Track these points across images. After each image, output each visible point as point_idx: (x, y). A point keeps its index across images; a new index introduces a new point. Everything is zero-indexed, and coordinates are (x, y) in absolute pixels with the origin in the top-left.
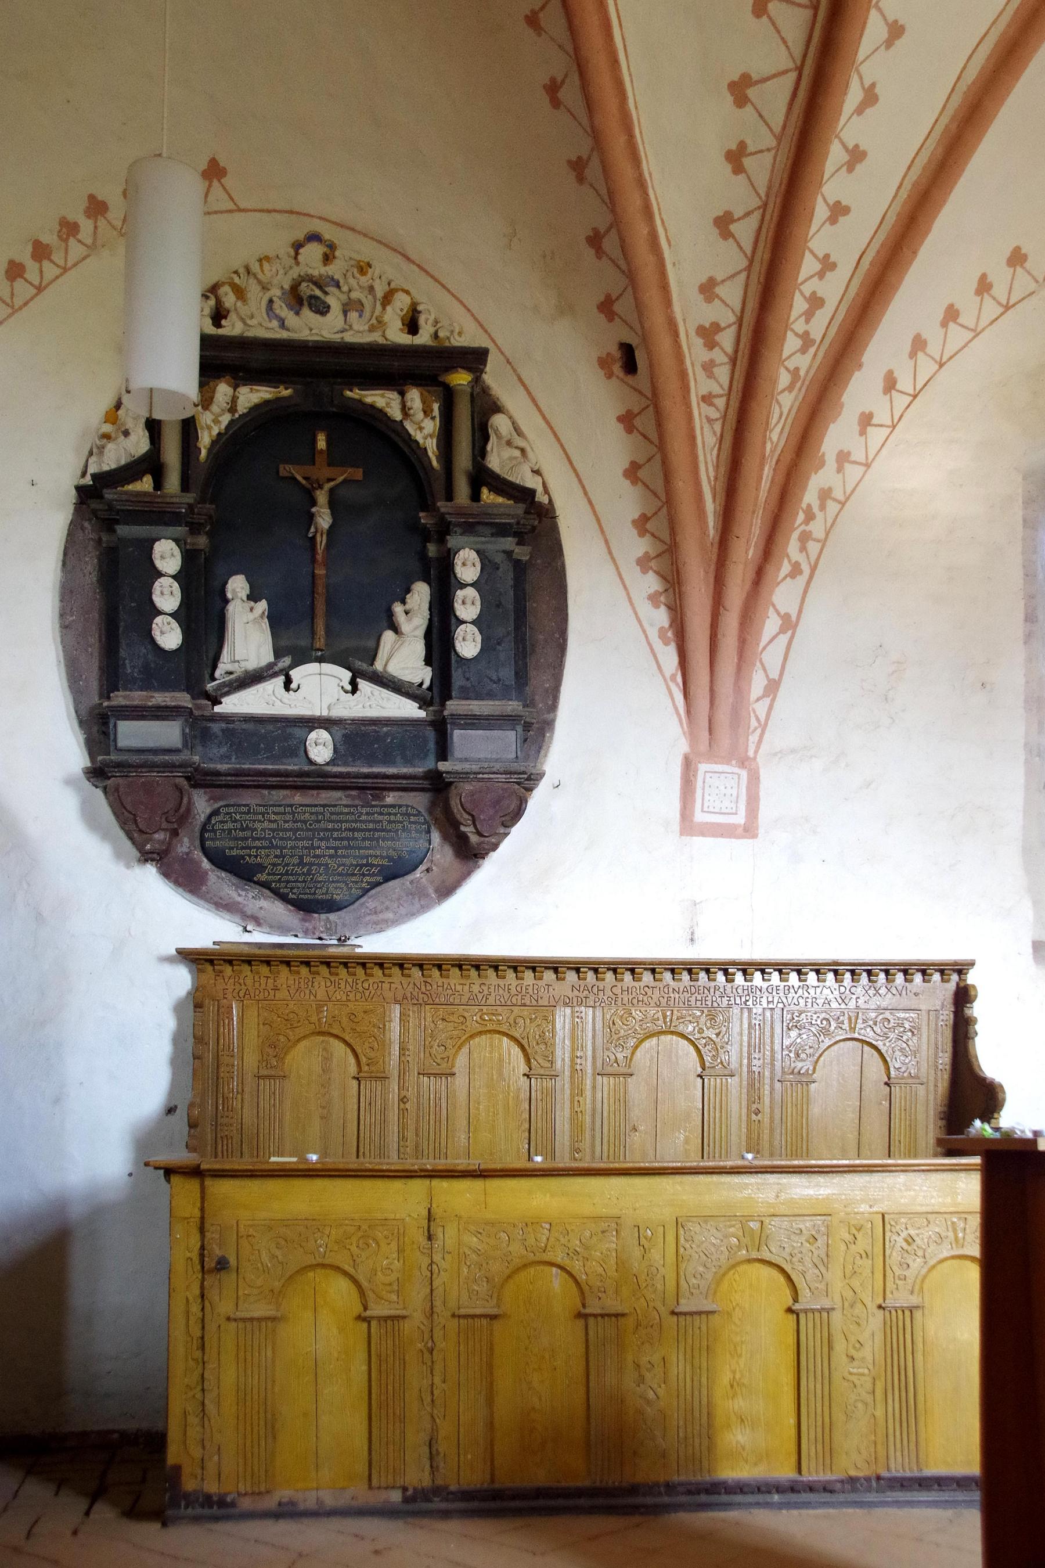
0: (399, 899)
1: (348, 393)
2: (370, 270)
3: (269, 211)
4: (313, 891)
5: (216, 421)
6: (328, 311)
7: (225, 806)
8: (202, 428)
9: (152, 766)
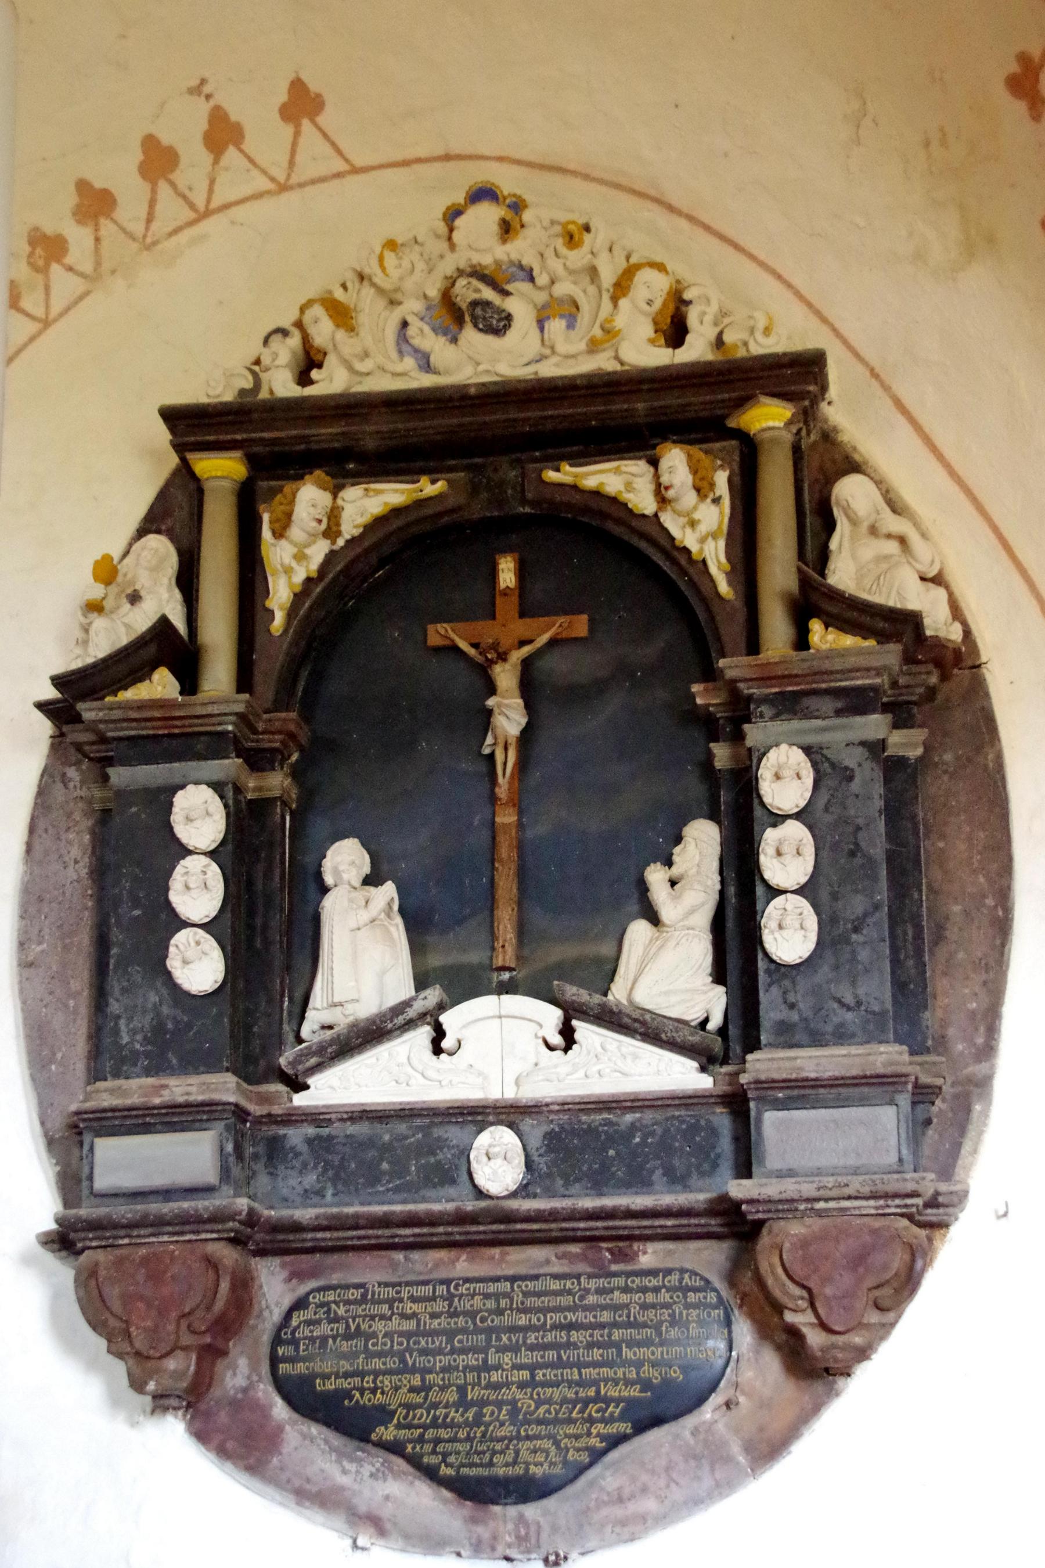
0: (668, 1469)
1: (551, 475)
2: (587, 238)
3: (406, 163)
4: (487, 1458)
5: (300, 557)
6: (507, 327)
7: (319, 1290)
8: (275, 573)
9: (159, 1223)
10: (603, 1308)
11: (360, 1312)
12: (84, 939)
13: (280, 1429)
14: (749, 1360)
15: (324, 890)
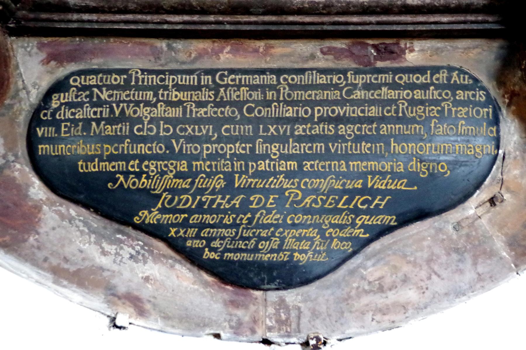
0: (429, 261)
7: (80, 73)
10: (372, 102)
11: (124, 97)
13: (37, 208)
14: (515, 158)
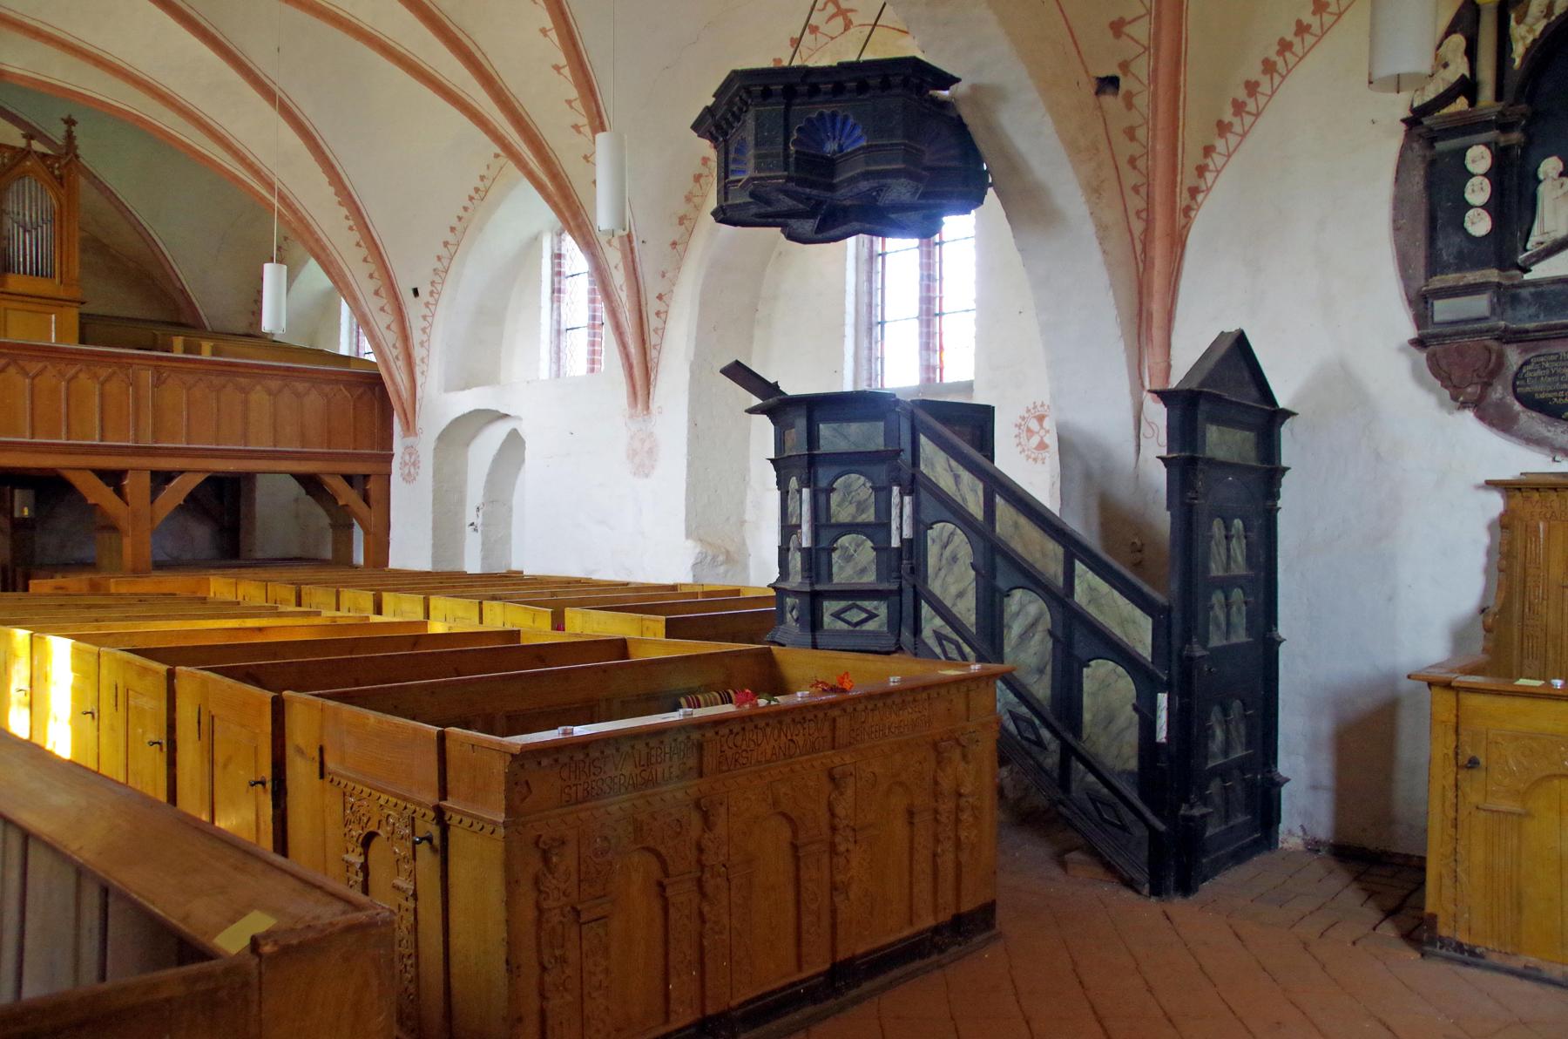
5: (1531, 30)
9: (1464, 333)
12: (1422, 216)
15: (1540, 182)
